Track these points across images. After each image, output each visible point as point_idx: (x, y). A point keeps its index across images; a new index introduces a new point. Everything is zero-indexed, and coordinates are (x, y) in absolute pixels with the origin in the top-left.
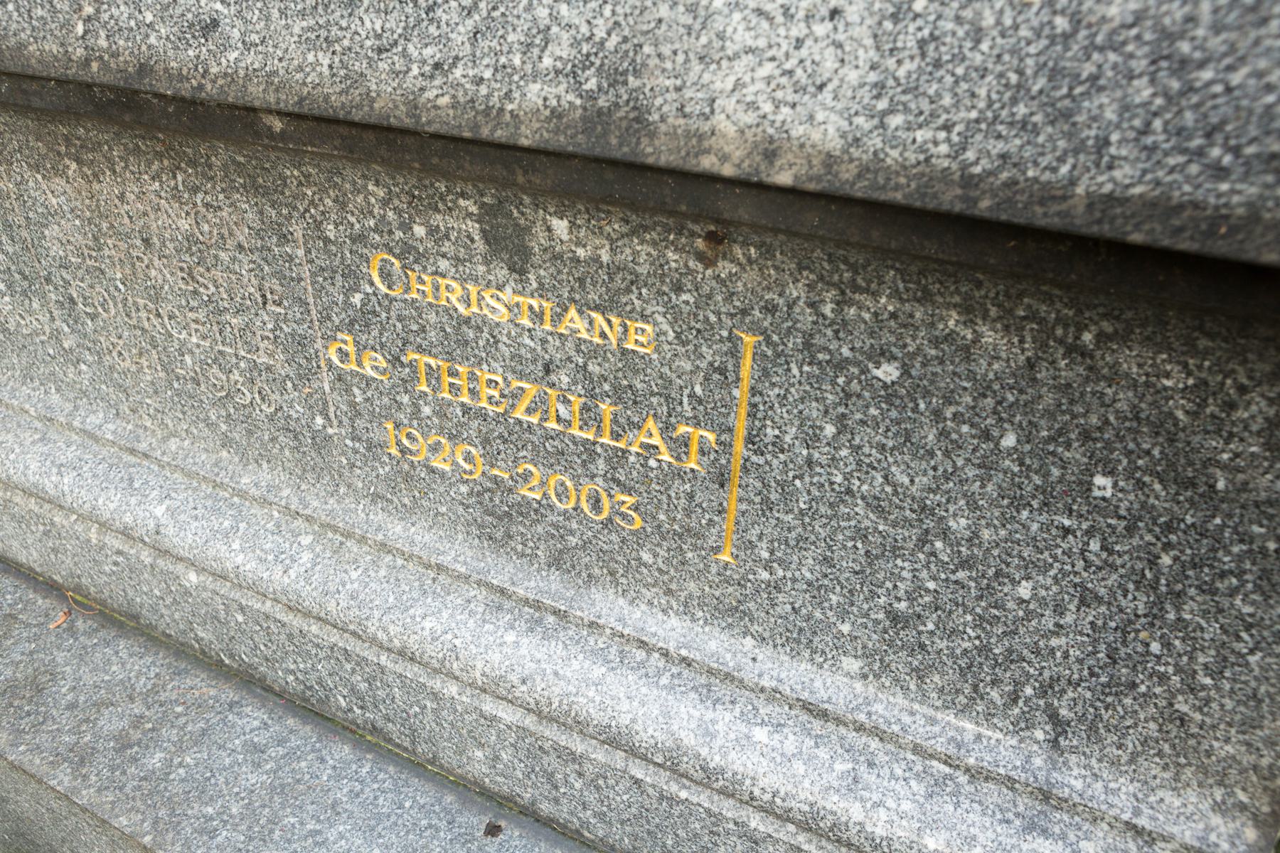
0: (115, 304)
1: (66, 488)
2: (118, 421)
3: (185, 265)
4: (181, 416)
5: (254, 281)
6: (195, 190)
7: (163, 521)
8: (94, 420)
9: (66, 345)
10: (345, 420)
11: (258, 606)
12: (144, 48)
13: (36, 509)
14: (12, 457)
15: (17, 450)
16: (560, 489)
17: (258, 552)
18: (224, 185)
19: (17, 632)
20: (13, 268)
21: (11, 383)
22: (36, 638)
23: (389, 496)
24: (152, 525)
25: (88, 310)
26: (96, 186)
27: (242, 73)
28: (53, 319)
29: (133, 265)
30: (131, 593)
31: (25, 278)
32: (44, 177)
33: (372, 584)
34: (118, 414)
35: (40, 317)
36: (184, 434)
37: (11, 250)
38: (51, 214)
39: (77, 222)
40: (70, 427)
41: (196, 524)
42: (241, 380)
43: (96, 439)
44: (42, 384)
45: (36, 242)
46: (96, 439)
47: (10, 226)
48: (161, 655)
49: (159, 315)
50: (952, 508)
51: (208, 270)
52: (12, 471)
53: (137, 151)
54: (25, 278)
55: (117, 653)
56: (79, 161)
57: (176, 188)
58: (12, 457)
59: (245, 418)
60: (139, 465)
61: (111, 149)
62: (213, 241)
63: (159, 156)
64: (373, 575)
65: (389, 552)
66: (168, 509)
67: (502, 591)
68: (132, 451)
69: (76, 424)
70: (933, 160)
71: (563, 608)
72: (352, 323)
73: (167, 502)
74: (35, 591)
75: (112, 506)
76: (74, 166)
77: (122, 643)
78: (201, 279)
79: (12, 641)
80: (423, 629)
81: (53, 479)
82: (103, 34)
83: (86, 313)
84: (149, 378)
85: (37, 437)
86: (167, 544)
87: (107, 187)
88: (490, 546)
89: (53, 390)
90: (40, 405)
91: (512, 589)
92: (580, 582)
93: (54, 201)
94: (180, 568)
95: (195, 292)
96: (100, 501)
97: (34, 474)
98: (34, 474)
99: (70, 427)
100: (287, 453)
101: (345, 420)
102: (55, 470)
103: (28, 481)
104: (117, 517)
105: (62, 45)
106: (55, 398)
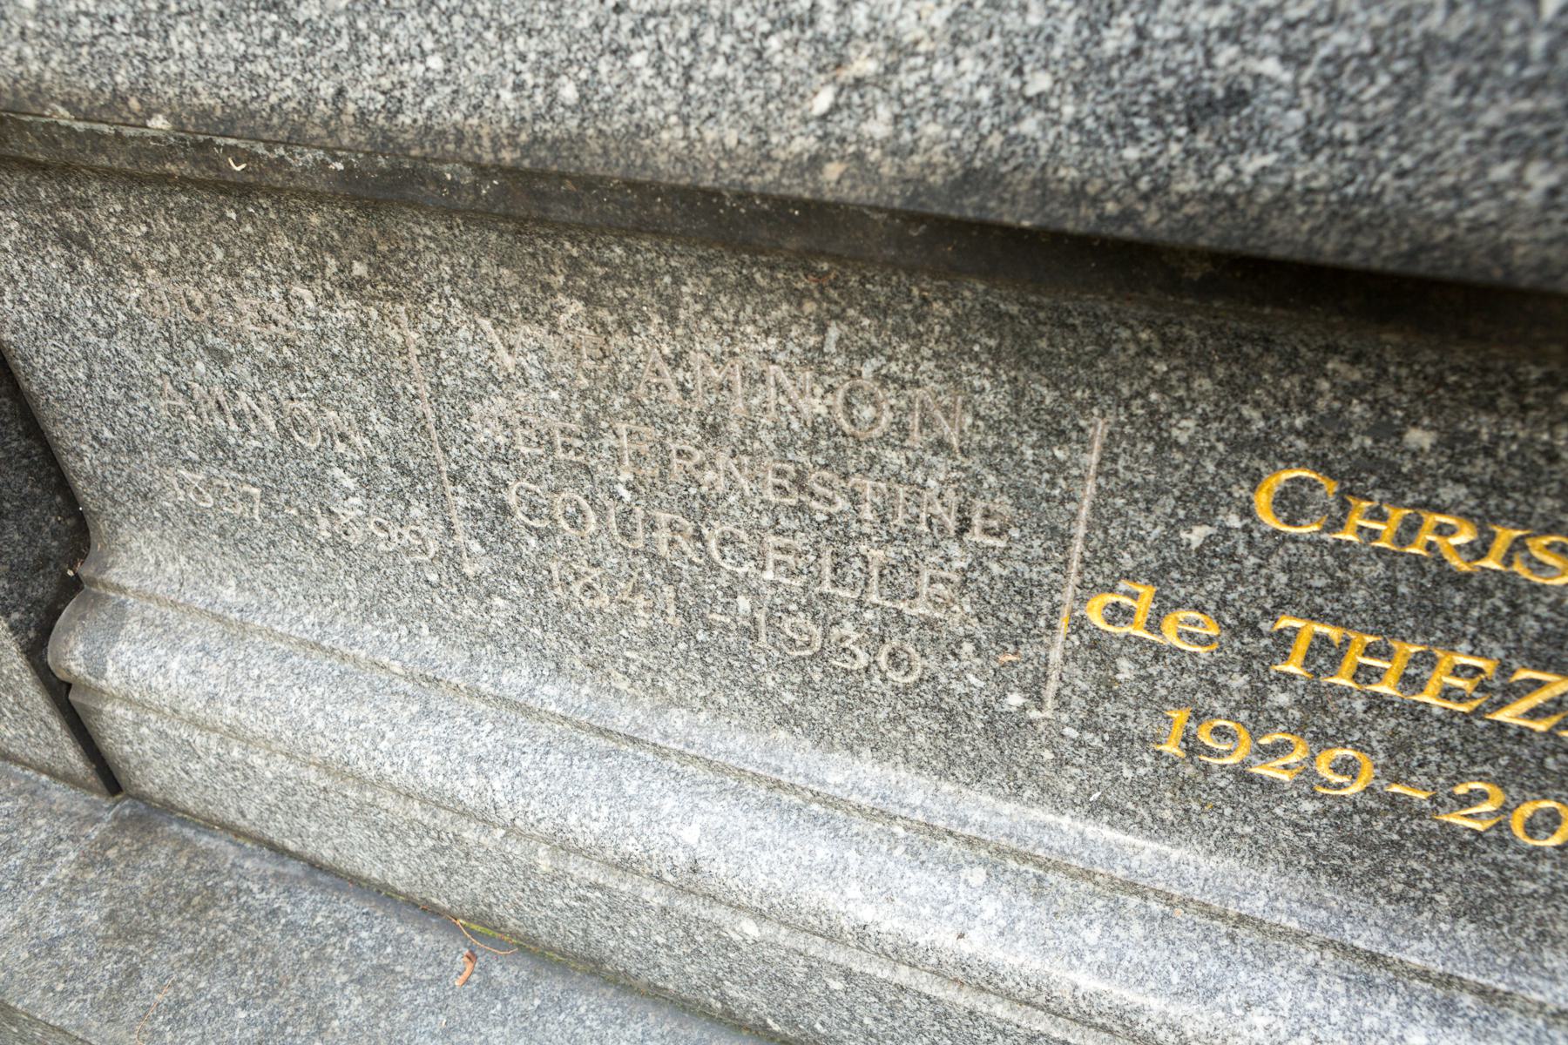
0: (602, 518)
1: (499, 797)
2: (561, 681)
3: (790, 468)
4: (698, 678)
5: (950, 495)
6: (866, 353)
7: (702, 852)
8: (515, 680)
9: (469, 570)
10: (1077, 702)
11: (885, 974)
12: (995, 140)
13: (427, 819)
14: (383, 746)
15: (390, 735)
16: (571, 510)
17: (898, 901)
18: (942, 348)
19: (405, 998)
20: (382, 457)
21: (341, 619)
22: (441, 1005)
23: (1130, 806)
24: (681, 858)
25: (536, 523)
26: (619, 340)
27: (1266, 194)
28: (450, 529)
29: (666, 463)
30: (597, 933)
31: (404, 471)
32: (497, 323)
33: (1130, 953)
34: (558, 668)
35: (424, 530)
36: (697, 704)
37: (384, 431)
38: (494, 380)
39: (554, 395)
40: (474, 692)
41: (766, 856)
42: (855, 636)
43: (527, 711)
44: (401, 621)
45: (446, 421)
46: (527, 711)
47: (395, 396)
48: (652, 1018)
49: (698, 536)
50: (204, 271)
51: (846, 476)
52: (388, 769)
53: (747, 285)
54: (404, 471)
55: (580, 1020)
56: (589, 299)
57: (820, 349)
58: (383, 746)
59: (852, 694)
60: (617, 751)
61: (678, 281)
62: (876, 433)
63: (798, 297)
64: (1123, 935)
65: (1137, 893)
66: (704, 830)
67: (1373, 958)
68: (603, 732)
69: (485, 687)
70: (395, 19)
71: (1502, 987)
72: (1164, 569)
73: (699, 819)
74: (401, 921)
75: (597, 828)
76: (577, 307)
77: (582, 1003)
78: (819, 489)
79: (405, 1015)
80: (1252, 1028)
81: (473, 782)
82: (884, 112)
83: (529, 529)
84: (643, 624)
85: (415, 708)
86: (713, 886)
87: (648, 344)
88: (1331, 883)
89: (425, 631)
90: (407, 657)
91: (1397, 955)
92: (1520, 941)
93: (509, 361)
94: (721, 914)
95: (800, 508)
96: (572, 819)
97: (434, 775)
98: (434, 775)
99: (474, 692)
100: (921, 738)
101: (1077, 702)
102: (471, 768)
103: (423, 785)
104: (607, 843)
105: (756, 129)
106: (430, 643)
